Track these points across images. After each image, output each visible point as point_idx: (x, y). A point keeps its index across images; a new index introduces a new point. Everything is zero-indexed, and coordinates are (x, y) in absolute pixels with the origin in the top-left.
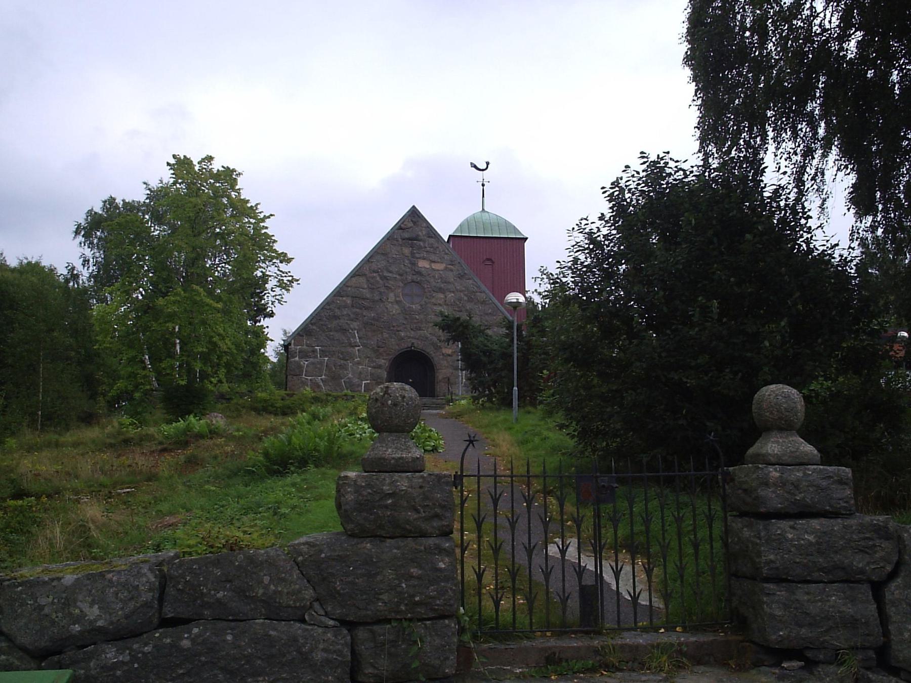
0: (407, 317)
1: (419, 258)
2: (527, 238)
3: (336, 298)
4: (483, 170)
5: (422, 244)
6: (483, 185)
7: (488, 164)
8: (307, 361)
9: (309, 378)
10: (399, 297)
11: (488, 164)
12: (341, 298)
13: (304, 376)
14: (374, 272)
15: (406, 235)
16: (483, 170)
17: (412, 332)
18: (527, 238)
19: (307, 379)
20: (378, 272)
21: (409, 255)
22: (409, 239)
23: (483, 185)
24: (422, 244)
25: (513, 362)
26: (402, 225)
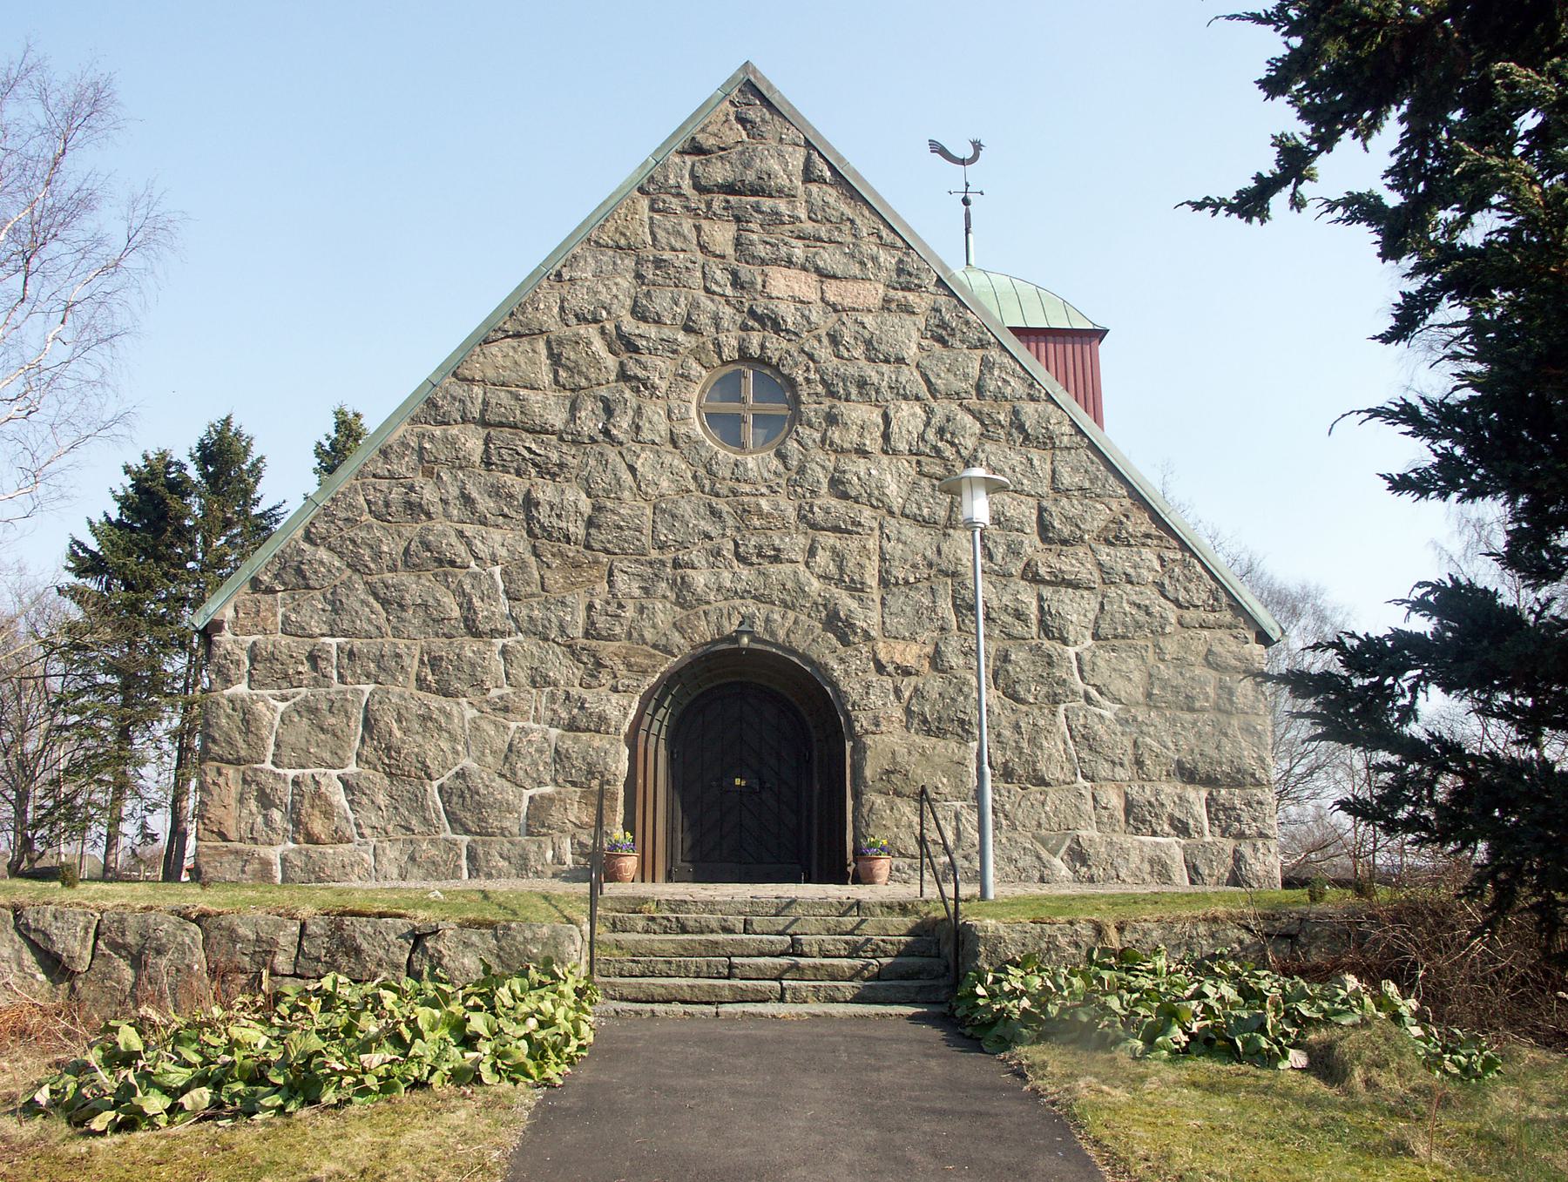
0: (721, 505)
1: (775, 262)
2: (1106, 331)
3: (418, 429)
4: (962, 162)
5: (782, 206)
6: (966, 202)
7: (977, 146)
8: (284, 699)
9: (291, 773)
10: (683, 419)
11: (977, 146)
12: (438, 431)
13: (268, 765)
14: (581, 318)
15: (719, 172)
16: (962, 162)
17: (745, 572)
18: (1106, 331)
19: (277, 776)
20: (596, 321)
21: (730, 251)
22: (729, 189)
23: (966, 202)
24: (782, 206)
25: (892, 1003)
26: (699, 137)
